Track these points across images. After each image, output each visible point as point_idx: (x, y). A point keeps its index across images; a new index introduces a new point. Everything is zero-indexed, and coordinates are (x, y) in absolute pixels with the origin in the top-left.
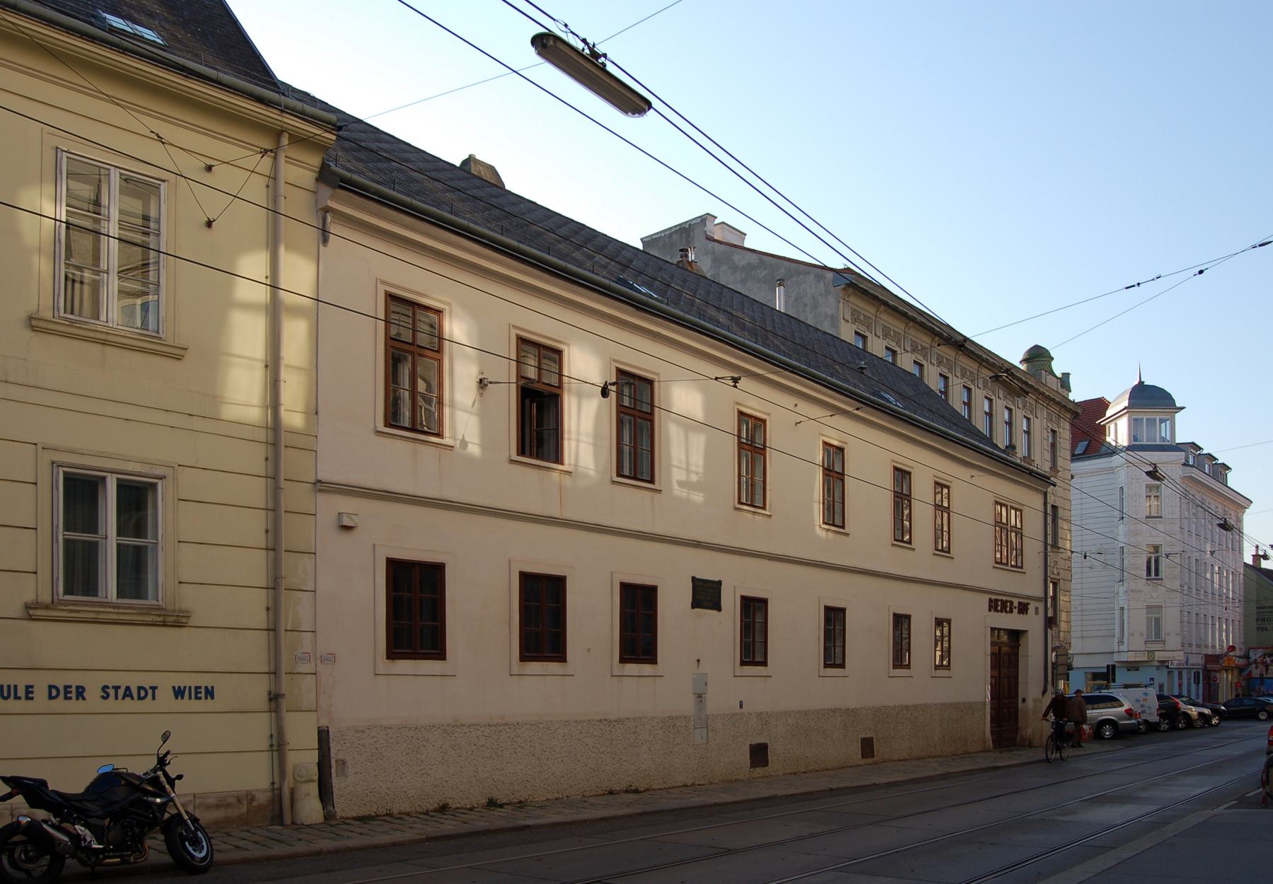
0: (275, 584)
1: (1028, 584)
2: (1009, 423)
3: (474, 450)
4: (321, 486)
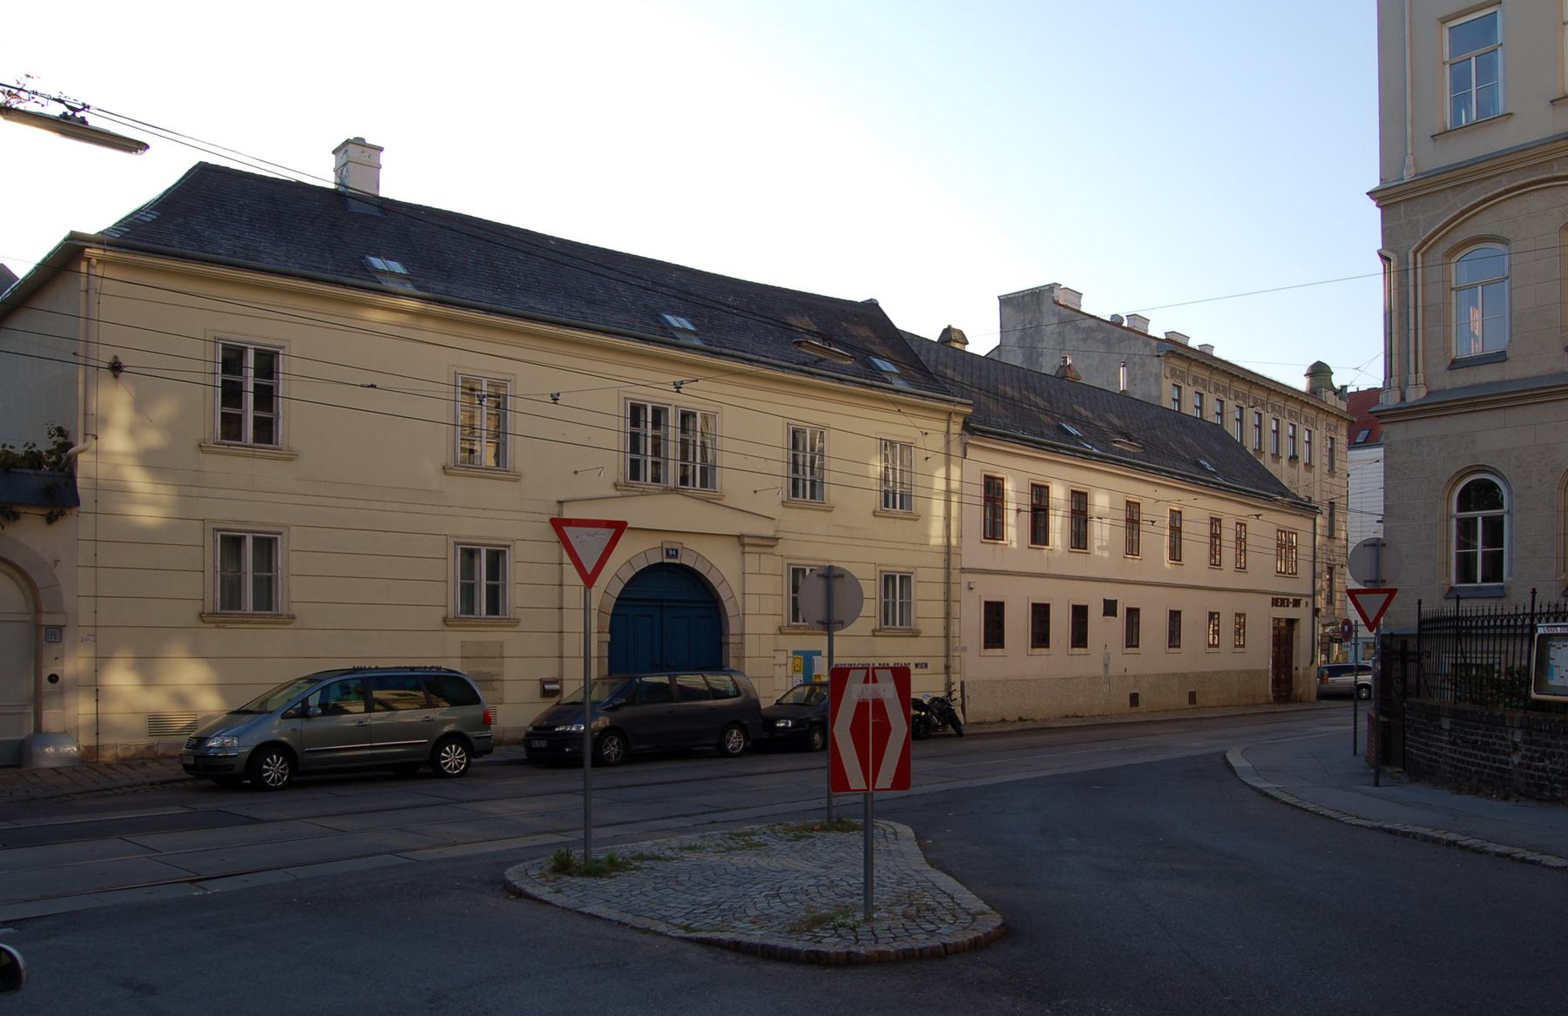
0: (948, 616)
1: (1301, 586)
2: (1293, 437)
3: (1014, 545)
4: (963, 570)
